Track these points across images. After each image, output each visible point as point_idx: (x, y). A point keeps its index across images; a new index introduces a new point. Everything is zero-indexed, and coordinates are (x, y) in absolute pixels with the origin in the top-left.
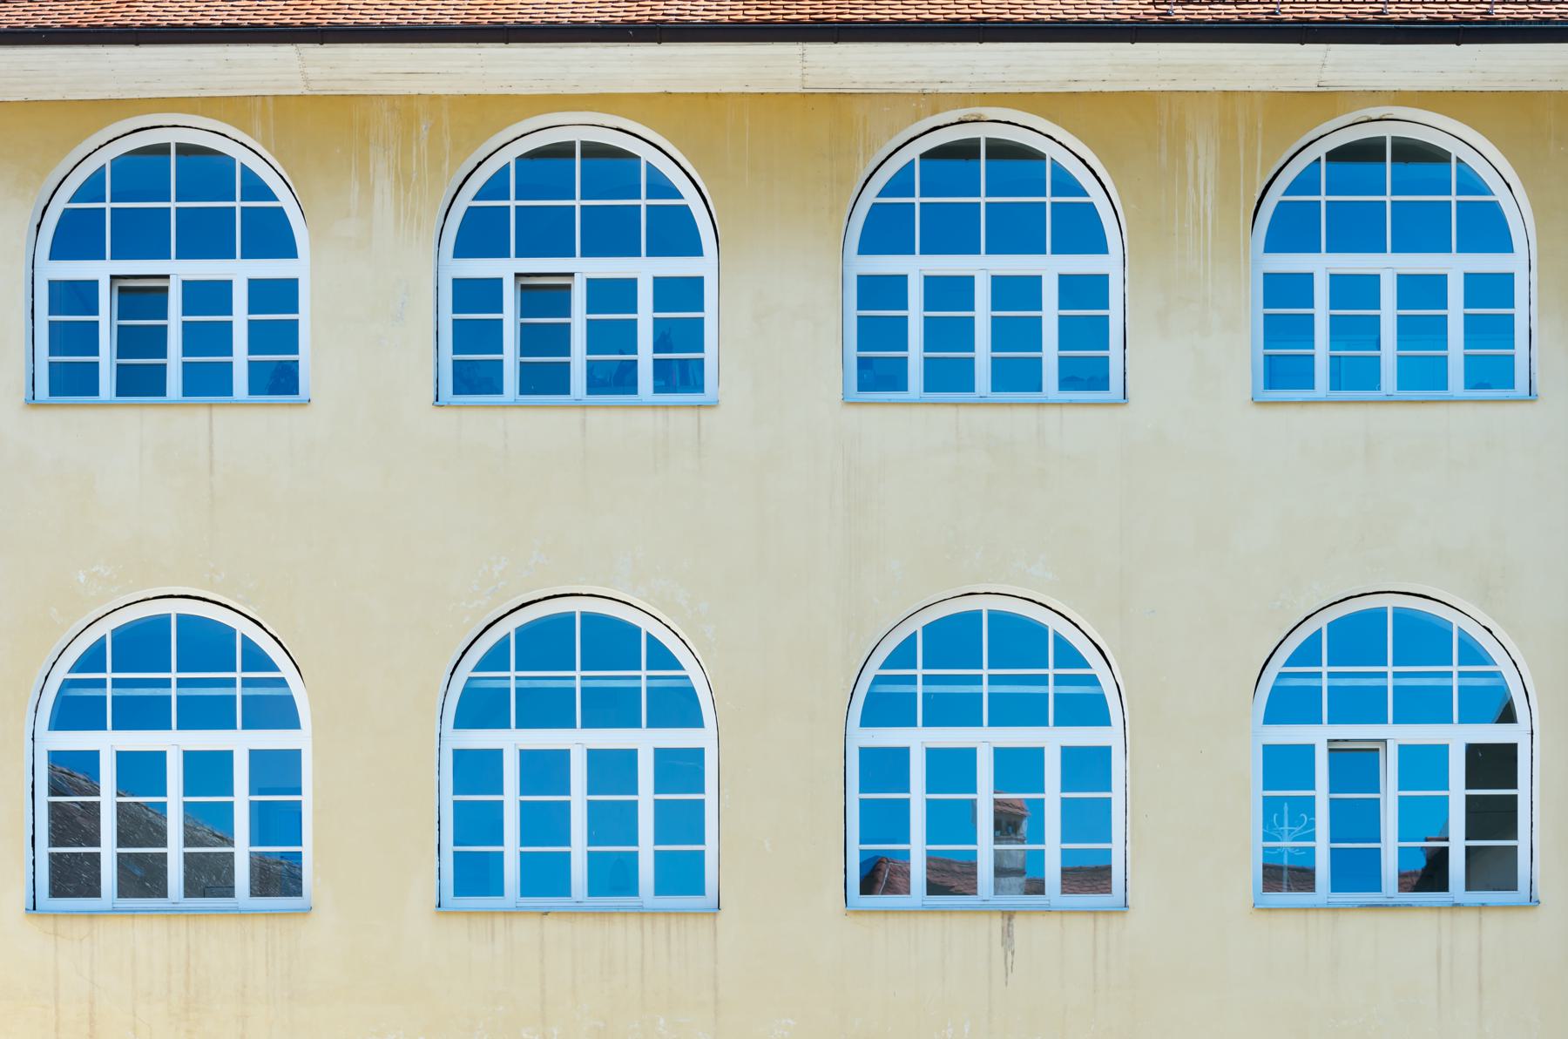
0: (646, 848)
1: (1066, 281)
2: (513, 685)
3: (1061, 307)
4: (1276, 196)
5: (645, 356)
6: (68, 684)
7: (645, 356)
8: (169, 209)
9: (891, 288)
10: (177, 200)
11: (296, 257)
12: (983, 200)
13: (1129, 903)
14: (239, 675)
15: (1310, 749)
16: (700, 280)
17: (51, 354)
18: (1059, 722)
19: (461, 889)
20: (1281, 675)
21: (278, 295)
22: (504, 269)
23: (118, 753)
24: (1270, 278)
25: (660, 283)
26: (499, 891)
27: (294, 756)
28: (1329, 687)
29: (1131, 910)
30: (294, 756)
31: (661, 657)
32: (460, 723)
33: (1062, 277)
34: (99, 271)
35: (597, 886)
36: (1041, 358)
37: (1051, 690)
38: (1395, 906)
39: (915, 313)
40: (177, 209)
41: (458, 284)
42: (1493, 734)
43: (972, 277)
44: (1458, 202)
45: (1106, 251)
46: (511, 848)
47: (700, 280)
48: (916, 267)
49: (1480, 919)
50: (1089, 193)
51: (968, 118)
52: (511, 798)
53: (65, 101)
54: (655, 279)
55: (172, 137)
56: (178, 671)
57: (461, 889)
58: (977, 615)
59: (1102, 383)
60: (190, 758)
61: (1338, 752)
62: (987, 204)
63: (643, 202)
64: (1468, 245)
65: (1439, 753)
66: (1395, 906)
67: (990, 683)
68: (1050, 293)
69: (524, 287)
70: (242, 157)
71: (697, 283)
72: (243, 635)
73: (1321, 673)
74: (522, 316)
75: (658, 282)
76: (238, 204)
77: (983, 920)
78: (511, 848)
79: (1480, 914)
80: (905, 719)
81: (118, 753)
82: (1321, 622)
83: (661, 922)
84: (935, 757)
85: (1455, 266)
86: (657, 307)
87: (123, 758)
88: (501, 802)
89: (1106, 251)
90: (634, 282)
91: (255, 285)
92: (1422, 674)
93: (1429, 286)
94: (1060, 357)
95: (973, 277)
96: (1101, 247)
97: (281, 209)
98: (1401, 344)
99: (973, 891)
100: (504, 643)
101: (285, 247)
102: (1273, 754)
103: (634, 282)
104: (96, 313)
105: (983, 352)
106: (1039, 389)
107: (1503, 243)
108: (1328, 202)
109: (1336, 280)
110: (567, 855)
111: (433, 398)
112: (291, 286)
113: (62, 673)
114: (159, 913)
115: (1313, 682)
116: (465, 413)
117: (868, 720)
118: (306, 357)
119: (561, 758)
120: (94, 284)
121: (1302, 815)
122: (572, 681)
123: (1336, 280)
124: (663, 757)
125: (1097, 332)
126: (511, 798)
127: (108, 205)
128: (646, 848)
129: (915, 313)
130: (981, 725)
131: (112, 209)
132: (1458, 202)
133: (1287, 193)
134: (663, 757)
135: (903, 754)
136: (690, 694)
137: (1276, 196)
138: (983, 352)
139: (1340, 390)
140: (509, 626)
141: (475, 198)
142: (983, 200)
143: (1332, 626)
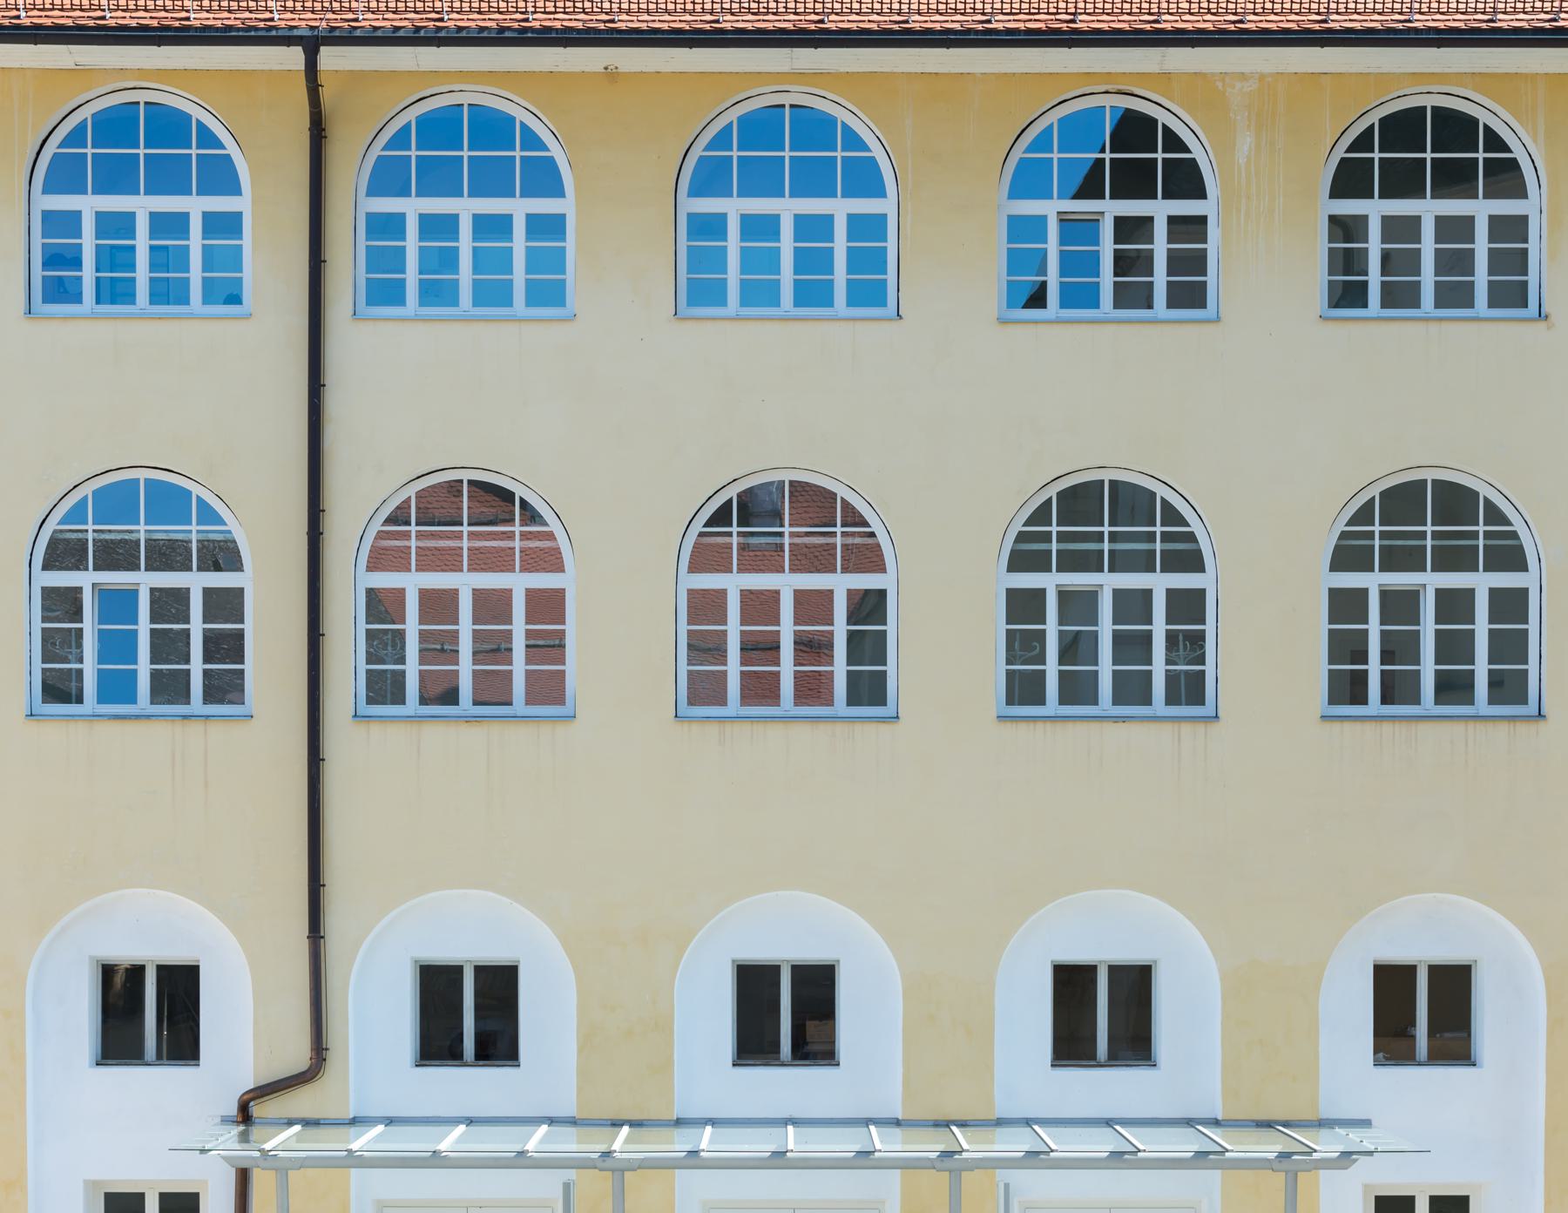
0: (1052, 668)
1: (1494, 220)
2: (194, 537)
3: (1490, 242)
4: (697, 152)
5: (1374, 278)
7: (1374, 278)
8: (1373, 159)
10: (93, 147)
11: (241, 195)
13: (1219, 715)
14: (413, 528)
15: (1365, 592)
16: (240, 214)
17: (1008, 275)
18: (524, 569)
20: (701, 534)
21: (1512, 228)
23: (1474, 589)
25: (853, 219)
27: (239, 593)
28: (1051, 542)
29: (901, 720)
30: (239, 593)
33: (529, 216)
36: (242, 278)
37: (1106, 546)
38: (148, 717)
39: (840, 244)
40: (1380, 159)
41: (370, 217)
42: (544, 581)
43: (1419, 217)
44: (197, 155)
45: (240, 193)
46: (519, 666)
47: (240, 214)
48: (88, 205)
49: (206, 730)
50: (227, 147)
51: (1111, 91)
52: (519, 627)
54: (528, 215)
56: (1051, 525)
61: (1064, 596)
62: (1380, 159)
63: (1160, 156)
65: (131, 594)
66: (148, 717)
67: (1110, 541)
68: (142, 226)
69: (1061, 220)
71: (237, 217)
72: (1162, 497)
73: (732, 532)
78: (519, 666)
79: (206, 724)
80: (79, 564)
81: (1474, 589)
82: (87, 490)
84: (748, 597)
87: (208, 593)
88: (1044, 631)
89: (240, 193)
90: (831, 217)
93: (119, 224)
94: (1489, 281)
95: (135, 213)
96: (559, 192)
97: (1194, 160)
102: (1336, 595)
103: (831, 217)
105: (1428, 278)
106: (1472, 306)
108: (469, 157)
109: (1440, 221)
111: (352, 312)
114: (83, 718)
115: (829, 540)
116: (1446, 326)
117: (694, 568)
120: (1044, 218)
121: (1035, 643)
122: (188, 535)
123: (1440, 221)
124: (532, 596)
125: (1519, 261)
126: (519, 627)
127: (89, 151)
128: (1159, 667)
129: (840, 244)
130: (1155, 571)
131: (1059, 158)
132: (197, 155)
133: (706, 149)
134: (532, 596)
135: (1040, 594)
136: (1520, 550)
137: (697, 152)
138: (1428, 278)
139: (168, 304)
141: (1347, 151)
142: (194, 152)
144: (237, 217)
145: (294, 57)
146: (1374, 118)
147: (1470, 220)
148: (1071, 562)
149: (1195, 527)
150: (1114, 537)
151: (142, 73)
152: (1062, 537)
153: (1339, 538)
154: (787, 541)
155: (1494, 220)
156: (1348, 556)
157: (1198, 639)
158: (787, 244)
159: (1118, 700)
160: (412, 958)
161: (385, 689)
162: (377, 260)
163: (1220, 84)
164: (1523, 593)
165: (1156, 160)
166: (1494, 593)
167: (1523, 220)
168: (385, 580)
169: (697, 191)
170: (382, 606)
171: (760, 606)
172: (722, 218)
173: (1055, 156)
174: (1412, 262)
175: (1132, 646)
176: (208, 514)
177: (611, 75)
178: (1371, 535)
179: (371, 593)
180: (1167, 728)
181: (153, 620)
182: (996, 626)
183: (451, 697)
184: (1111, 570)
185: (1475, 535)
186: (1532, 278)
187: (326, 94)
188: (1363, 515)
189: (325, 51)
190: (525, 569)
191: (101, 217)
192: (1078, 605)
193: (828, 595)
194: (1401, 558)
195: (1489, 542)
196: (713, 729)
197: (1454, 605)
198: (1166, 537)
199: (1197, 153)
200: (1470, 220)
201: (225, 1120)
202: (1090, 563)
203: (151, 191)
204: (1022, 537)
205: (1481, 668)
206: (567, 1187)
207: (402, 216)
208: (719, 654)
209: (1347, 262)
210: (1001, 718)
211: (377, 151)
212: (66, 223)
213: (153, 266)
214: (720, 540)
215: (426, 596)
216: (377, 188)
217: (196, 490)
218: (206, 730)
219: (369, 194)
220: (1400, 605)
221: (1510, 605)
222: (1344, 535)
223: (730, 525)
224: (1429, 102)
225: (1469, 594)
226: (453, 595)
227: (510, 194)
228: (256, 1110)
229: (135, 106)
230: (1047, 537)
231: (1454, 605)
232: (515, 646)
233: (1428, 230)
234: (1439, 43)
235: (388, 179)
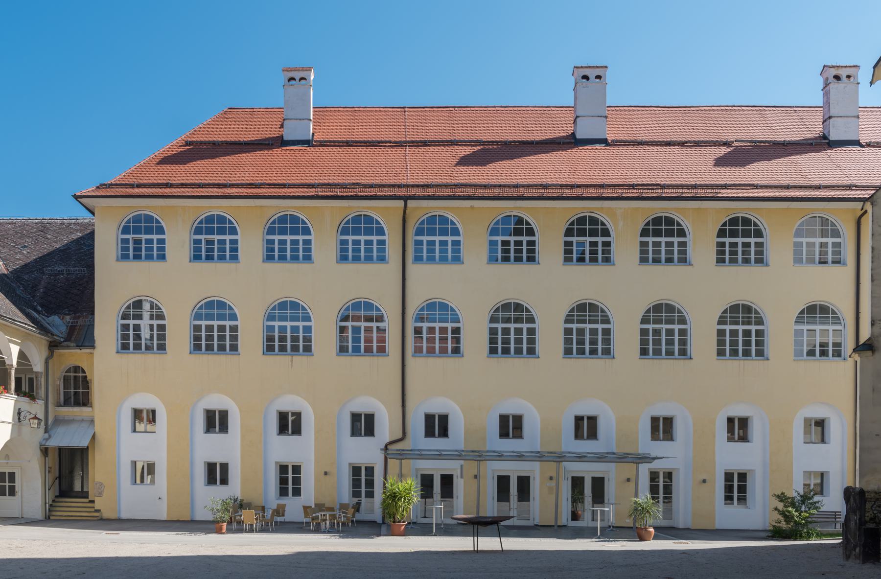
4: (342, 225)
6: (124, 311)
9: (346, 242)
12: (227, 225)
14: (155, 310)
19: (268, 350)
22: (202, 237)
24: (795, 243)
25: (230, 240)
26: (725, 356)
27: (310, 327)
30: (310, 327)
31: (230, 308)
32: (415, 322)
34: (130, 237)
35: (135, 349)
37: (289, 314)
42: (456, 325)
48: (277, 238)
49: (292, 360)
52: (228, 334)
53: (429, 207)
55: (437, 214)
57: (268, 350)
58: (287, 301)
59: (534, 260)
60: (304, 327)
64: (832, 237)
67: (589, 317)
68: (289, 243)
70: (375, 217)
71: (384, 241)
74: (206, 245)
75: (440, 241)
76: (301, 225)
77: (287, 357)
78: (216, 343)
80: (673, 323)
82: (350, 303)
83: (230, 356)
85: (375, 238)
86: (303, 245)
90: (522, 241)
91: (230, 240)
92: (369, 313)
93: (432, 243)
98: (452, 253)
99: (164, 352)
100: (202, 305)
101: (309, 233)
102: (718, 331)
104: (121, 246)
107: (384, 234)
109: (666, 243)
110: (360, 346)
112: (237, 240)
113: (123, 309)
115: (498, 316)
118: (313, 254)
119: (737, 331)
120: (129, 239)
123: (666, 243)
127: (204, 225)
136: (310, 317)
140: (203, 302)
143: (352, 304)
144: (384, 241)
145: (401, 203)
146: (650, 218)
147: (673, 242)
148: (578, 322)
149: (608, 313)
150: (589, 316)
151: (364, 208)
152: (290, 313)
153: (719, 318)
154: (512, 316)
155: (528, 242)
156: (645, 320)
158: (450, 247)
159: (577, 354)
160: (523, 415)
161: (418, 351)
162: (416, 251)
163: (615, 210)
164: (609, 329)
165: (664, 228)
167: (237, 240)
168: (419, 324)
169: (342, 234)
172: (274, 240)
173: (155, 225)
174: (285, 250)
176: (378, 309)
177: (472, 207)
178: (650, 316)
179: (415, 328)
180: (603, 360)
181: (230, 332)
182: (715, 338)
183: (584, 353)
184: (589, 323)
185: (499, 315)
186: (688, 256)
187: (408, 212)
189: (409, 202)
191: (292, 241)
192: (581, 332)
193: (298, 327)
194: (658, 321)
195: (439, 316)
196: (496, 359)
197: (519, 331)
198: (602, 316)
199: (608, 226)
200: (673, 242)
201: (381, 449)
202: (584, 322)
203: (279, 234)
204: (568, 316)
205: (500, 346)
206: (462, 466)
207: (286, 240)
209: (721, 253)
210: (563, 358)
211: (417, 225)
212: (345, 242)
213: (743, 255)
214: (285, 314)
216: (417, 234)
217: (375, 303)
218: (292, 360)
219: (340, 235)
220: (734, 333)
221: (531, 331)
222: (644, 316)
223: (373, 311)
224: (663, 215)
225: (725, 330)
227: (373, 235)
228: (389, 447)
229: (815, 218)
230: (650, 316)
231: (519, 331)
232: (451, 340)
233: (663, 245)
234: (801, 201)
235: (419, 232)
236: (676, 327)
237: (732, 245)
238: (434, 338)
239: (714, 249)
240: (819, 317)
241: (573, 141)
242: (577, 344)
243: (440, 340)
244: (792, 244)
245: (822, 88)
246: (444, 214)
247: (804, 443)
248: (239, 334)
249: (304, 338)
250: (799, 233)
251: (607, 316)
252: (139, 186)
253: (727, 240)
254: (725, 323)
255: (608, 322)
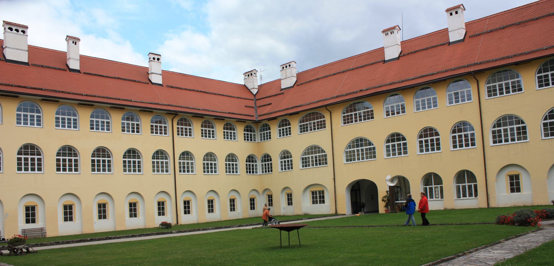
24: (56, 117)
80: (28, 155)
156: (19, 153)
157: (41, 164)
161: (180, 171)
166: (436, 139)
170: (180, 163)
171: (184, 163)
172: (59, 118)
175: (33, 164)
178: (212, 158)
182: (55, 163)
188: (21, 148)
190: (210, 161)
192: (64, 160)
197: (33, 160)
204: (19, 151)
207: (389, 145)
208: (60, 166)
212: (20, 115)
215: (69, 160)
225: (21, 158)
226: (60, 159)
236: (36, 157)
237: (25, 116)
238: (21, 163)
239: (89, 123)
240: (24, 151)
241: (4, 59)
242: (28, 163)
243: (60, 165)
244: (121, 123)
245: (3, 33)
246: (186, 118)
247: (442, 197)
248: (476, 141)
249: (95, 166)
250: (280, 127)
251: (40, 152)
252: (63, 92)
253: (390, 144)
254: (95, 157)
255: (40, 155)
